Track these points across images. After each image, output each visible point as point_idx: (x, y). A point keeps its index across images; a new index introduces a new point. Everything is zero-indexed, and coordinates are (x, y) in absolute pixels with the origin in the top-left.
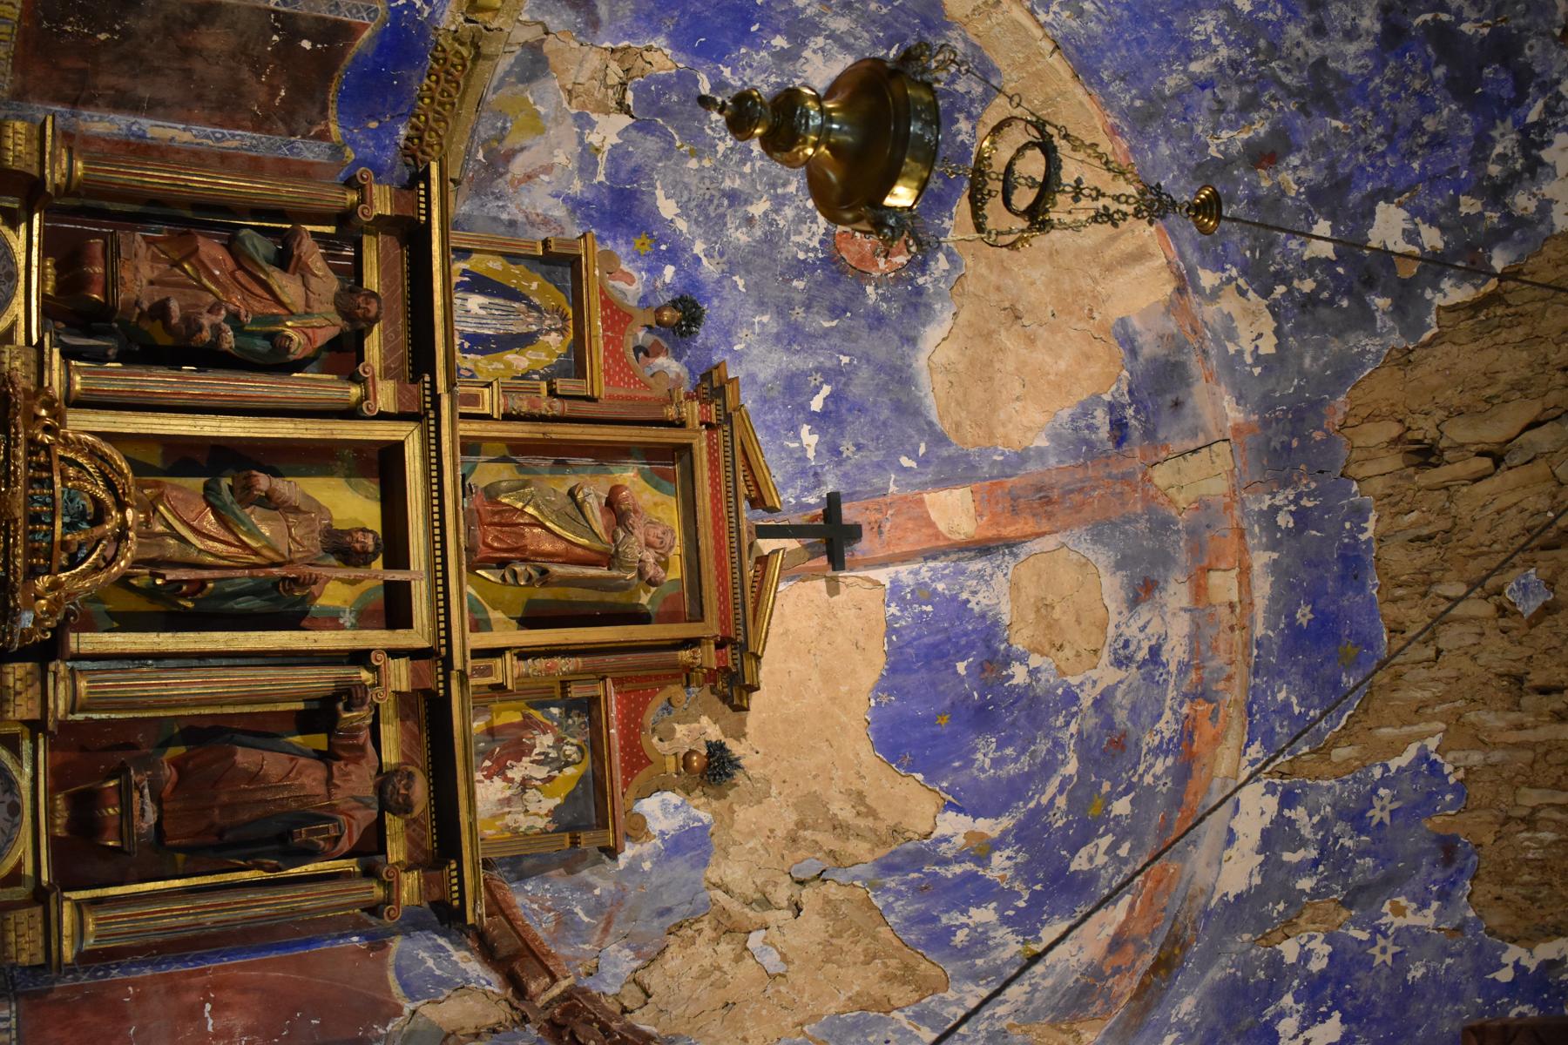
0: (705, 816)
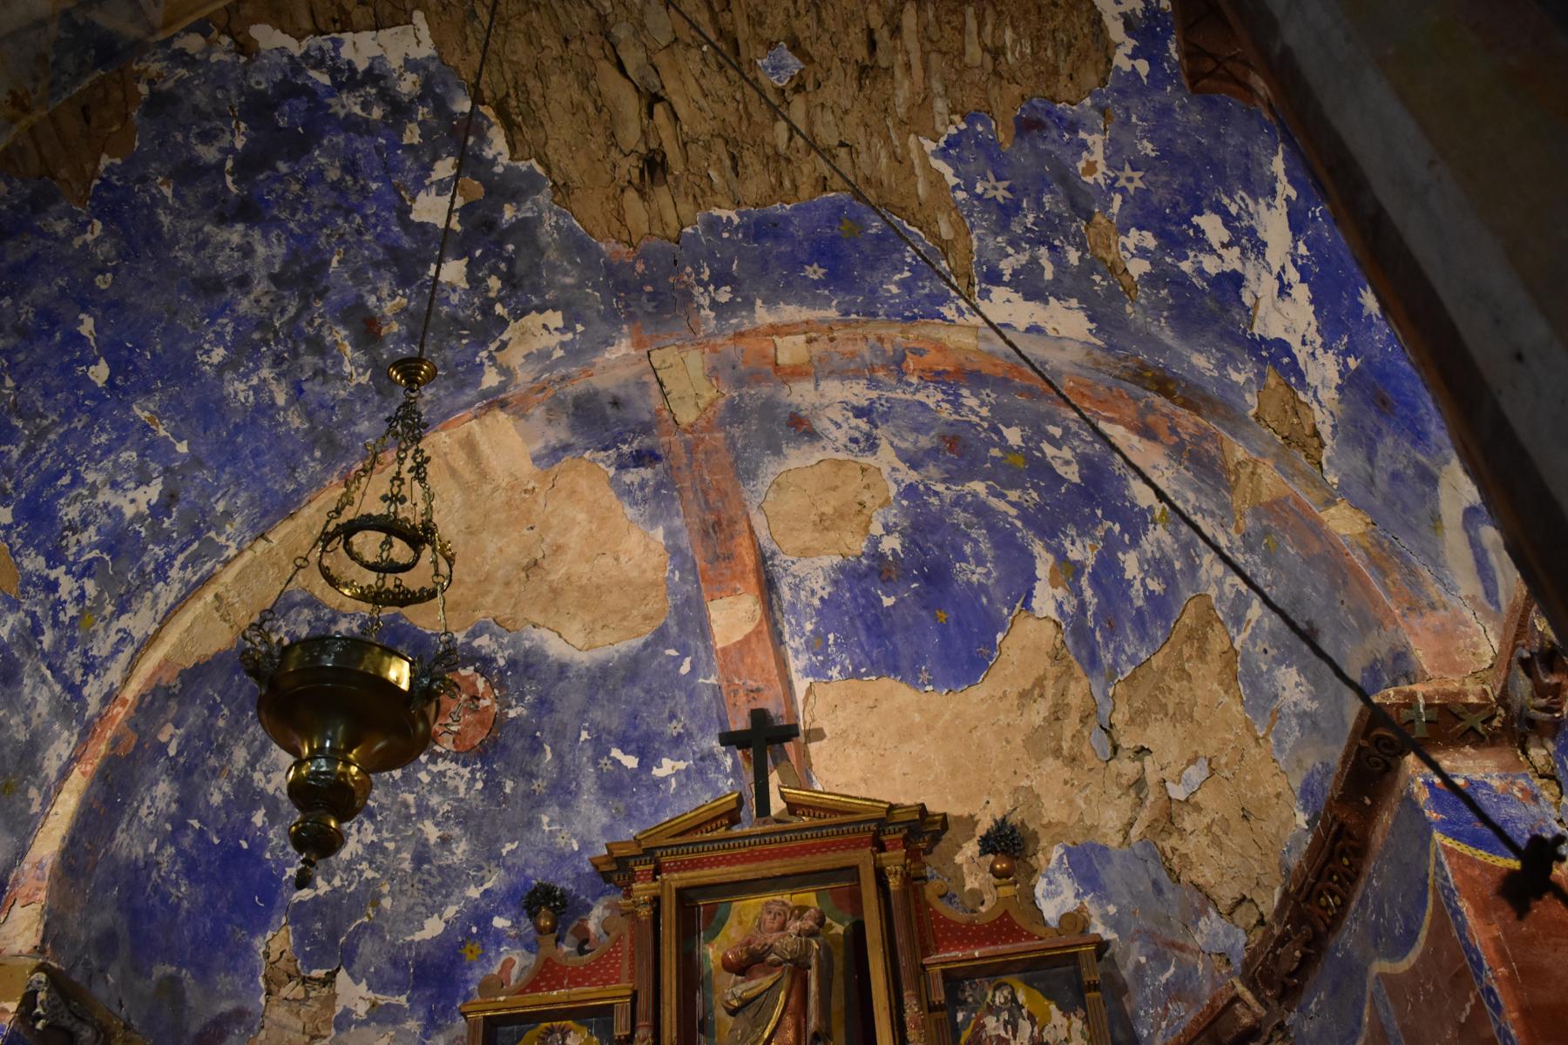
0: (1056, 852)
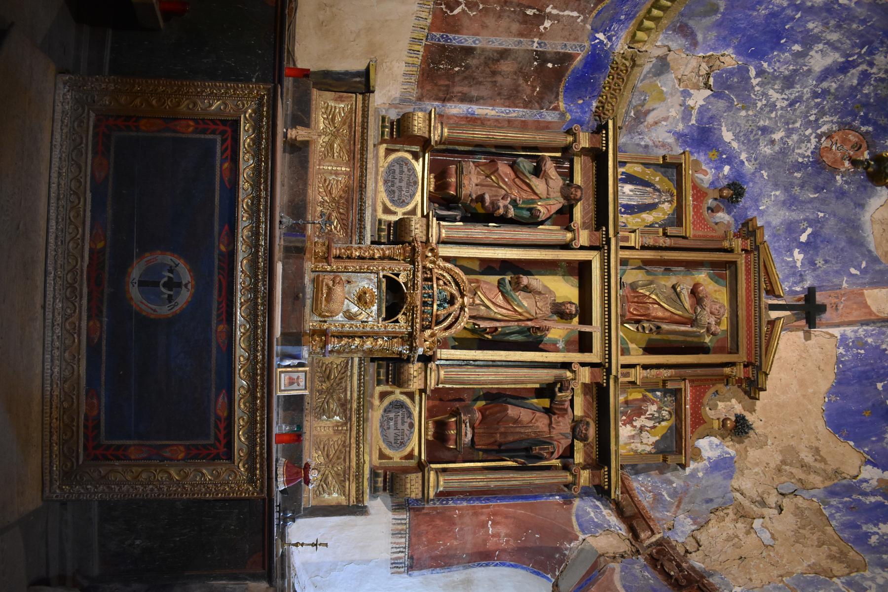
0: (732, 452)
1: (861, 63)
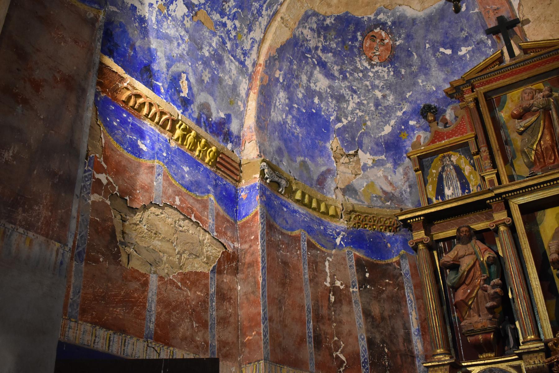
1: (317, 55)
